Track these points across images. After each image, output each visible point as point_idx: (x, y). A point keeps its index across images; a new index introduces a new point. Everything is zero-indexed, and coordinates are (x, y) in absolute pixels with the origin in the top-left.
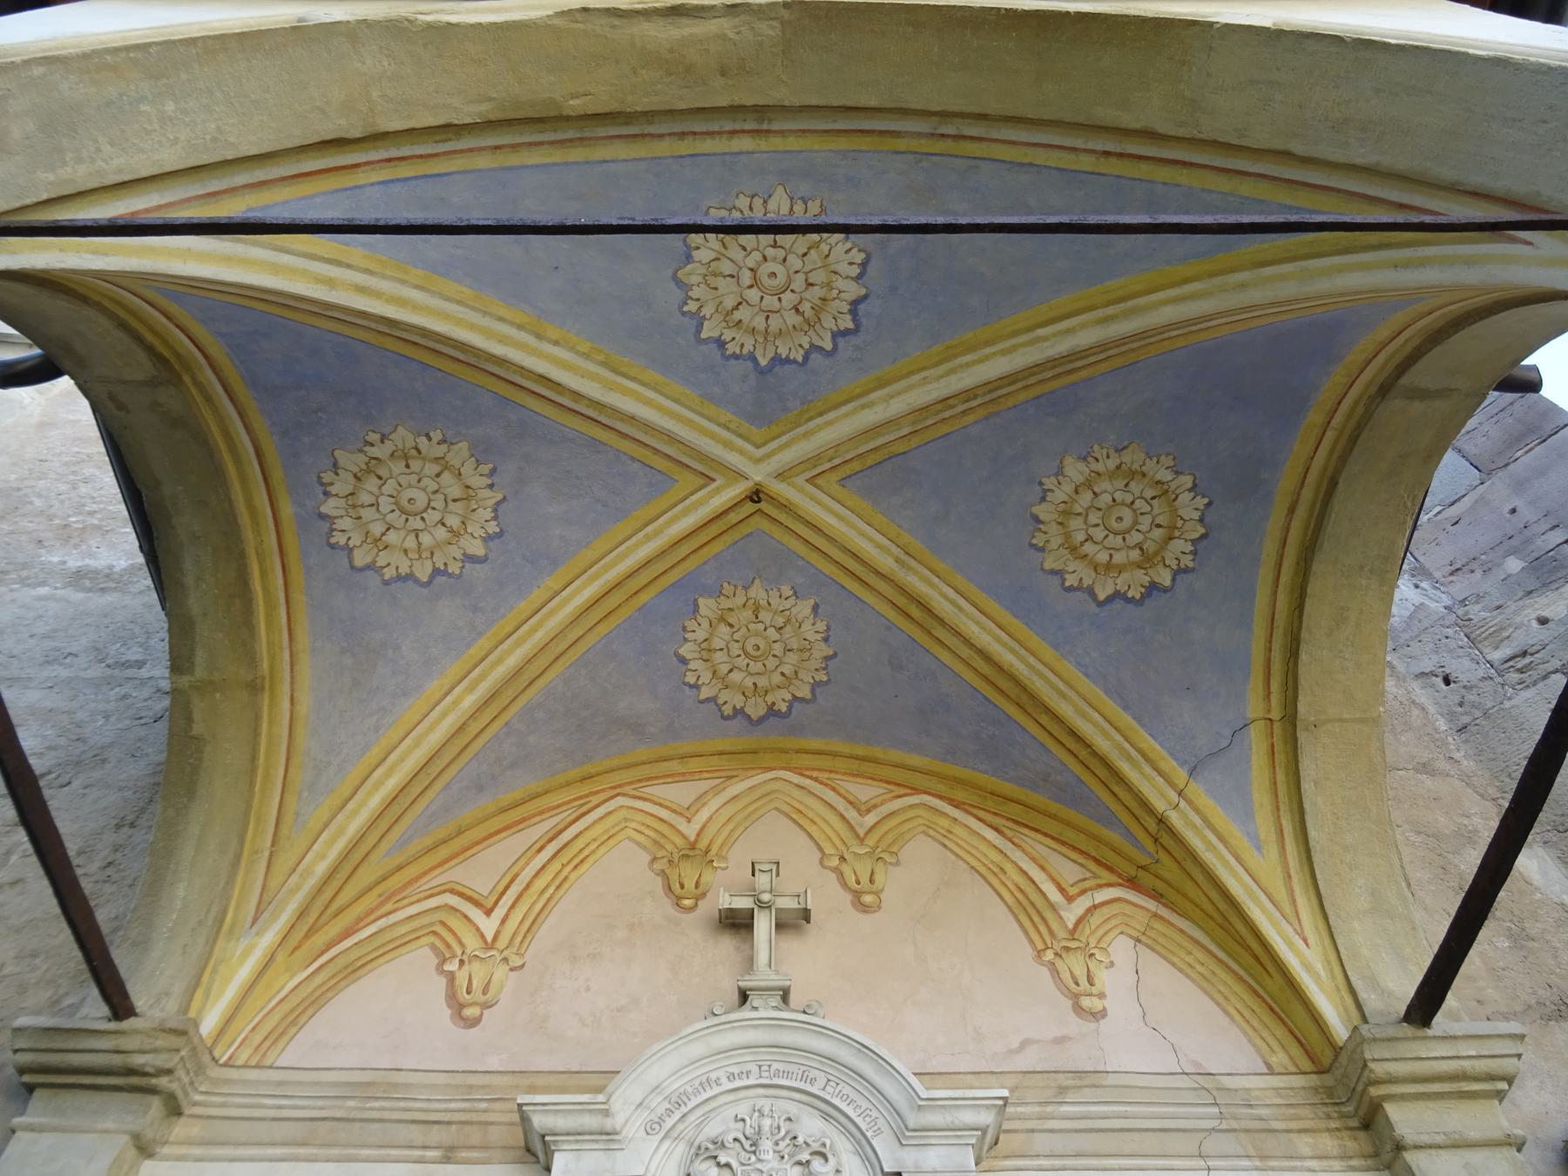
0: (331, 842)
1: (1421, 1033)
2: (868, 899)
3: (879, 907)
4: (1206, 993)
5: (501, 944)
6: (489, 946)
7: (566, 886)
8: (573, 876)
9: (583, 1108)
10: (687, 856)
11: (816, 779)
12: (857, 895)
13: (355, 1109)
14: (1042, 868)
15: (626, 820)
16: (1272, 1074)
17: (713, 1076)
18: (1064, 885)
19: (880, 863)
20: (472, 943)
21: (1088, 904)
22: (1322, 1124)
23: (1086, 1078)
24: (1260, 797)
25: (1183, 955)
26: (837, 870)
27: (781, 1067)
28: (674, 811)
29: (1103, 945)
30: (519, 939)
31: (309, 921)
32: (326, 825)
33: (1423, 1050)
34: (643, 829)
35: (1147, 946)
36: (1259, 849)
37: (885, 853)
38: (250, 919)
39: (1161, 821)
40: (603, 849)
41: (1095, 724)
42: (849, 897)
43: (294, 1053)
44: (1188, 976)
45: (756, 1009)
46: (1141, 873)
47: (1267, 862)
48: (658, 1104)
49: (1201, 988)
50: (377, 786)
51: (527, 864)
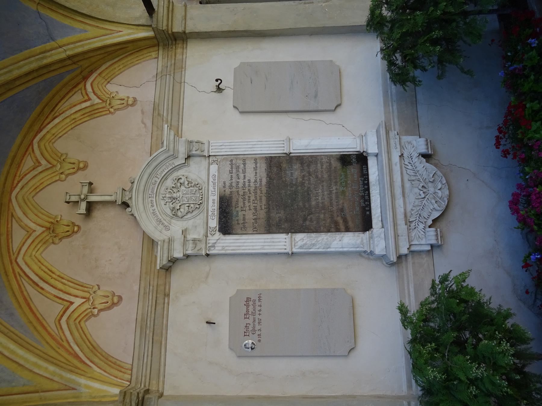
0: (39, 367)
1: (156, 12)
2: (81, 165)
3: (86, 162)
4: (130, 68)
5: (86, 295)
6: (88, 299)
7: (62, 275)
8: (58, 273)
9: (162, 248)
10: (53, 231)
11: (19, 182)
12: (79, 169)
13: (150, 330)
14: (75, 106)
15: (31, 256)
16: (158, 58)
17: (152, 211)
18: (83, 100)
19: (66, 160)
20: (86, 306)
21: (92, 94)
22: (174, 51)
23: (156, 108)
24: (67, 22)
25: (116, 71)
26: (67, 175)
27: (150, 191)
28: (28, 237)
29: (109, 93)
30: (86, 289)
31: (74, 370)
32: (31, 371)
33: (160, 15)
34: (36, 249)
35: (111, 80)
36: (86, 31)
37: (62, 158)
38: (75, 391)
39: (69, 58)
40: (45, 263)
41: (25, 65)
42: (80, 172)
43: (126, 358)
44: (124, 71)
45: (131, 198)
46: (83, 74)
47: (92, 31)
48: (160, 227)
49: (128, 69)
50: (13, 352)
51: (49, 293)
